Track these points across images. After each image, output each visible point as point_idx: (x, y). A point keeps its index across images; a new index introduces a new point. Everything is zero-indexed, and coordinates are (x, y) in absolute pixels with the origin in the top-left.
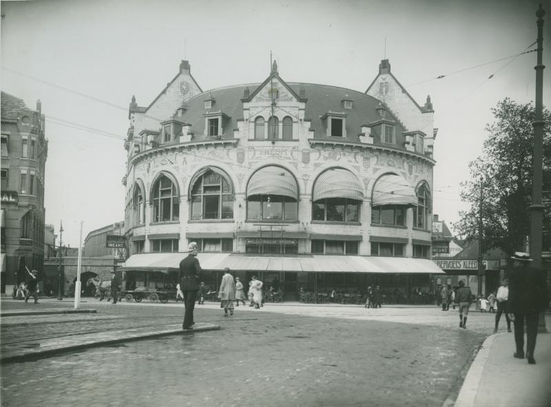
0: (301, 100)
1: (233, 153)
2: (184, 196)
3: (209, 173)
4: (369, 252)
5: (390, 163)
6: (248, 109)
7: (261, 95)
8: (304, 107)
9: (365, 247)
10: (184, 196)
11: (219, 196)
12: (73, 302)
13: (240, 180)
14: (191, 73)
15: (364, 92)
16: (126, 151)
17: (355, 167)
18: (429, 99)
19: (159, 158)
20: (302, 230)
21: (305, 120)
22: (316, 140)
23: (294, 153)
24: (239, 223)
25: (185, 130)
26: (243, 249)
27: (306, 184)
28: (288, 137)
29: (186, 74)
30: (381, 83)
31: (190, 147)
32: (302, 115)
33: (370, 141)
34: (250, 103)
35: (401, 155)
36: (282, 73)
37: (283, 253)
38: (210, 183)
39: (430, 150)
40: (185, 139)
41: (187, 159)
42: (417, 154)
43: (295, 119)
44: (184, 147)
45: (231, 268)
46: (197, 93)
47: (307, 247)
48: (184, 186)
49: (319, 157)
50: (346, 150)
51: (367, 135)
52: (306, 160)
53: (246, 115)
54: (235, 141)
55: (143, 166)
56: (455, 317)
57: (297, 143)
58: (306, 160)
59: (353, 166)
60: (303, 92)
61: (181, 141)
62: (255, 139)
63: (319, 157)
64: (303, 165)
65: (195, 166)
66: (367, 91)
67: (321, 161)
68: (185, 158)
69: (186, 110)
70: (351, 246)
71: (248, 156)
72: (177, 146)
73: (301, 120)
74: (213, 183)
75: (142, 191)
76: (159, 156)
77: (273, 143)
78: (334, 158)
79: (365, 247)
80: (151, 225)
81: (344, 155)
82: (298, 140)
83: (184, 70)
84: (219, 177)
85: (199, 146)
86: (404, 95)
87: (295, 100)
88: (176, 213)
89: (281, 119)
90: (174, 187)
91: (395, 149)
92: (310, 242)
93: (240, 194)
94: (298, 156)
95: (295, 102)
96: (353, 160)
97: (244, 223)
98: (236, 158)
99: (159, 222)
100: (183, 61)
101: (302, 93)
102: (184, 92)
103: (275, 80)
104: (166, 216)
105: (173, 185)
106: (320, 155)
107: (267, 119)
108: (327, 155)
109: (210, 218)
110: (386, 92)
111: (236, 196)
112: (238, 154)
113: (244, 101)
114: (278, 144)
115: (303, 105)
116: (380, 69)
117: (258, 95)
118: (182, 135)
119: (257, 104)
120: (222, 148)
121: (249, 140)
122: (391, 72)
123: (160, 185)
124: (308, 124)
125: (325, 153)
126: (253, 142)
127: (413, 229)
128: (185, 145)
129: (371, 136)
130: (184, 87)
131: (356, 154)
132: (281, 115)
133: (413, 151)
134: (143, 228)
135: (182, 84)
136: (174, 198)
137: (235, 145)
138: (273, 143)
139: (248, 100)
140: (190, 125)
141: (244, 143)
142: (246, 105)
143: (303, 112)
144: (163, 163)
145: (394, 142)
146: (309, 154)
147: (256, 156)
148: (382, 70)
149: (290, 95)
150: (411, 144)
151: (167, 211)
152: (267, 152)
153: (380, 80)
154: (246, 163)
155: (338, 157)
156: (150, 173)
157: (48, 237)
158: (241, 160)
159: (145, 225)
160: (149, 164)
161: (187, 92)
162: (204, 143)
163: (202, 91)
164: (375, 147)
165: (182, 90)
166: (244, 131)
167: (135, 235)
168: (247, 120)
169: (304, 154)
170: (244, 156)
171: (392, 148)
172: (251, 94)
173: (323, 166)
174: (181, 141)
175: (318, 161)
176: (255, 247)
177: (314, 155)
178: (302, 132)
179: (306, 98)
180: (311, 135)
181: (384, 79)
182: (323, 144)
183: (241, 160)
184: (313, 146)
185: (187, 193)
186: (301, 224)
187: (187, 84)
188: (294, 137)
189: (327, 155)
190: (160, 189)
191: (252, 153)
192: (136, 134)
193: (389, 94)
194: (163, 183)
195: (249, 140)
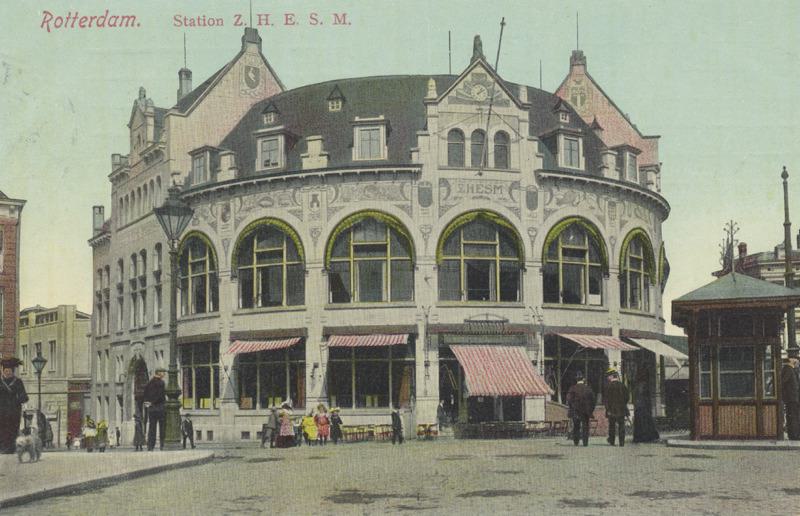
1: (411, 189)
7: (458, 93)
12: (373, 405)
13: (424, 234)
15: (553, 91)
22: (549, 171)
28: (503, 160)
41: (319, 198)
42: (623, 183)
48: (226, 253)
52: (532, 202)
57: (518, 175)
58: (532, 202)
59: (290, 211)
64: (529, 211)
66: (559, 90)
68: (315, 196)
89: (468, 134)
94: (520, 197)
100: (574, 52)
106: (552, 195)
114: (486, 175)
125: (561, 193)
130: (251, 75)
133: (617, 178)
135: (248, 68)
136: (349, 262)
141: (430, 175)
156: (231, 221)
165: (249, 81)
173: (559, 212)
174: (305, 167)
175: (336, 205)
177: (542, 195)
178: (526, 156)
182: (374, 172)
183: (425, 198)
184: (542, 181)
187: (256, 71)
194: (198, 244)
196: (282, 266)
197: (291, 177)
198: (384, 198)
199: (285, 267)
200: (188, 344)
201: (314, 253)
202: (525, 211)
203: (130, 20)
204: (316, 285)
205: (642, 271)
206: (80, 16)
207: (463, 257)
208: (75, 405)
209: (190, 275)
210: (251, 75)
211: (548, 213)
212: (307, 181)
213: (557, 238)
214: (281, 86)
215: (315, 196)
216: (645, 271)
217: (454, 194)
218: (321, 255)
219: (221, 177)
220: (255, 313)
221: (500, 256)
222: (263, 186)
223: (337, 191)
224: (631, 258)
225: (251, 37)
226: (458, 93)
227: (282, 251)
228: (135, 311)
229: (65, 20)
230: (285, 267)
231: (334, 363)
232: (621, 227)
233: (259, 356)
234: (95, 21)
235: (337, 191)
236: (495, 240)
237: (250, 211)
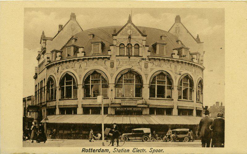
1: (108, 63)
2: (80, 85)
3: (95, 73)
4: (177, 114)
5: (186, 68)
8: (145, 39)
9: (80, 110)
10: (80, 85)
16: (37, 61)
17: (171, 71)
19: (65, 65)
21: (146, 46)
24: (112, 99)
25: (81, 50)
26: (113, 113)
27: (146, 79)
30: (176, 28)
31: (84, 60)
33: (178, 57)
35: (191, 64)
36: (134, 21)
37: (123, 114)
38: (94, 78)
39: (202, 62)
40: (80, 55)
43: (140, 45)
44: (75, 60)
45: (116, 123)
46: (80, 31)
47: (147, 112)
49: (153, 66)
50: (166, 61)
51: (176, 54)
54: (109, 56)
55: (55, 69)
56: (87, 142)
58: (146, 67)
60: (144, 31)
61: (78, 56)
62: (120, 56)
63: (153, 66)
66: (169, 31)
67: (154, 67)
69: (77, 39)
70: (169, 111)
71: (116, 64)
72: (76, 59)
73: (144, 46)
74: (96, 78)
75: (54, 82)
76: (64, 63)
77: (129, 58)
79: (80, 110)
80: (60, 100)
84: (100, 76)
85: (89, 59)
86: (188, 34)
87: (140, 35)
88: (76, 93)
90: (74, 80)
92: (149, 109)
95: (140, 36)
97: (114, 99)
98: (109, 65)
99: (65, 98)
101: (143, 32)
102: (73, 30)
103: (129, 25)
104: (69, 96)
105: (74, 79)
107: (126, 45)
108: (157, 64)
109: (72, 95)
110: (179, 32)
111: (110, 85)
113: (113, 35)
117: (121, 32)
118: (78, 53)
119: (120, 38)
120: (102, 60)
121: (116, 56)
122: (181, 22)
123: (65, 79)
125: (157, 63)
126: (119, 57)
127: (196, 102)
128: (81, 58)
129: (178, 55)
132: (133, 43)
134: (54, 102)
137: (109, 59)
138: (129, 58)
139: (116, 35)
140: (83, 48)
141: (113, 58)
144: (67, 67)
147: (120, 64)
149: (138, 33)
150: (195, 59)
151: (68, 93)
153: (175, 26)
156: (59, 73)
158: (112, 66)
159: (56, 100)
160: (58, 68)
162: (72, 59)
163: (82, 30)
166: (114, 51)
167: (48, 105)
168: (115, 45)
170: (114, 65)
172: (117, 32)
174: (78, 56)
175: (153, 67)
176: (121, 111)
179: (146, 34)
181: (177, 25)
183: (112, 66)
185: (82, 83)
186: (144, 100)
189: (157, 64)
190: (91, 79)
191: (118, 63)
192: (48, 51)
195: (116, 56)
196: (90, 85)
198: (166, 67)
199: (72, 87)
201: (80, 82)
202: (109, 68)
204: (81, 92)
205: (189, 87)
206: (93, 149)
208: (195, 112)
209: (65, 86)
211: (152, 69)
212: (78, 60)
213: (156, 76)
216: (190, 87)
217: (121, 63)
218: (148, 82)
219: (78, 55)
220: (90, 99)
222: (195, 67)
224: (183, 83)
225: (73, 16)
226: (123, 32)
227: (71, 82)
229: (89, 150)
230: (72, 87)
231: (91, 113)
232: (151, 71)
234: (97, 151)
236: (100, 78)
237: (64, 70)
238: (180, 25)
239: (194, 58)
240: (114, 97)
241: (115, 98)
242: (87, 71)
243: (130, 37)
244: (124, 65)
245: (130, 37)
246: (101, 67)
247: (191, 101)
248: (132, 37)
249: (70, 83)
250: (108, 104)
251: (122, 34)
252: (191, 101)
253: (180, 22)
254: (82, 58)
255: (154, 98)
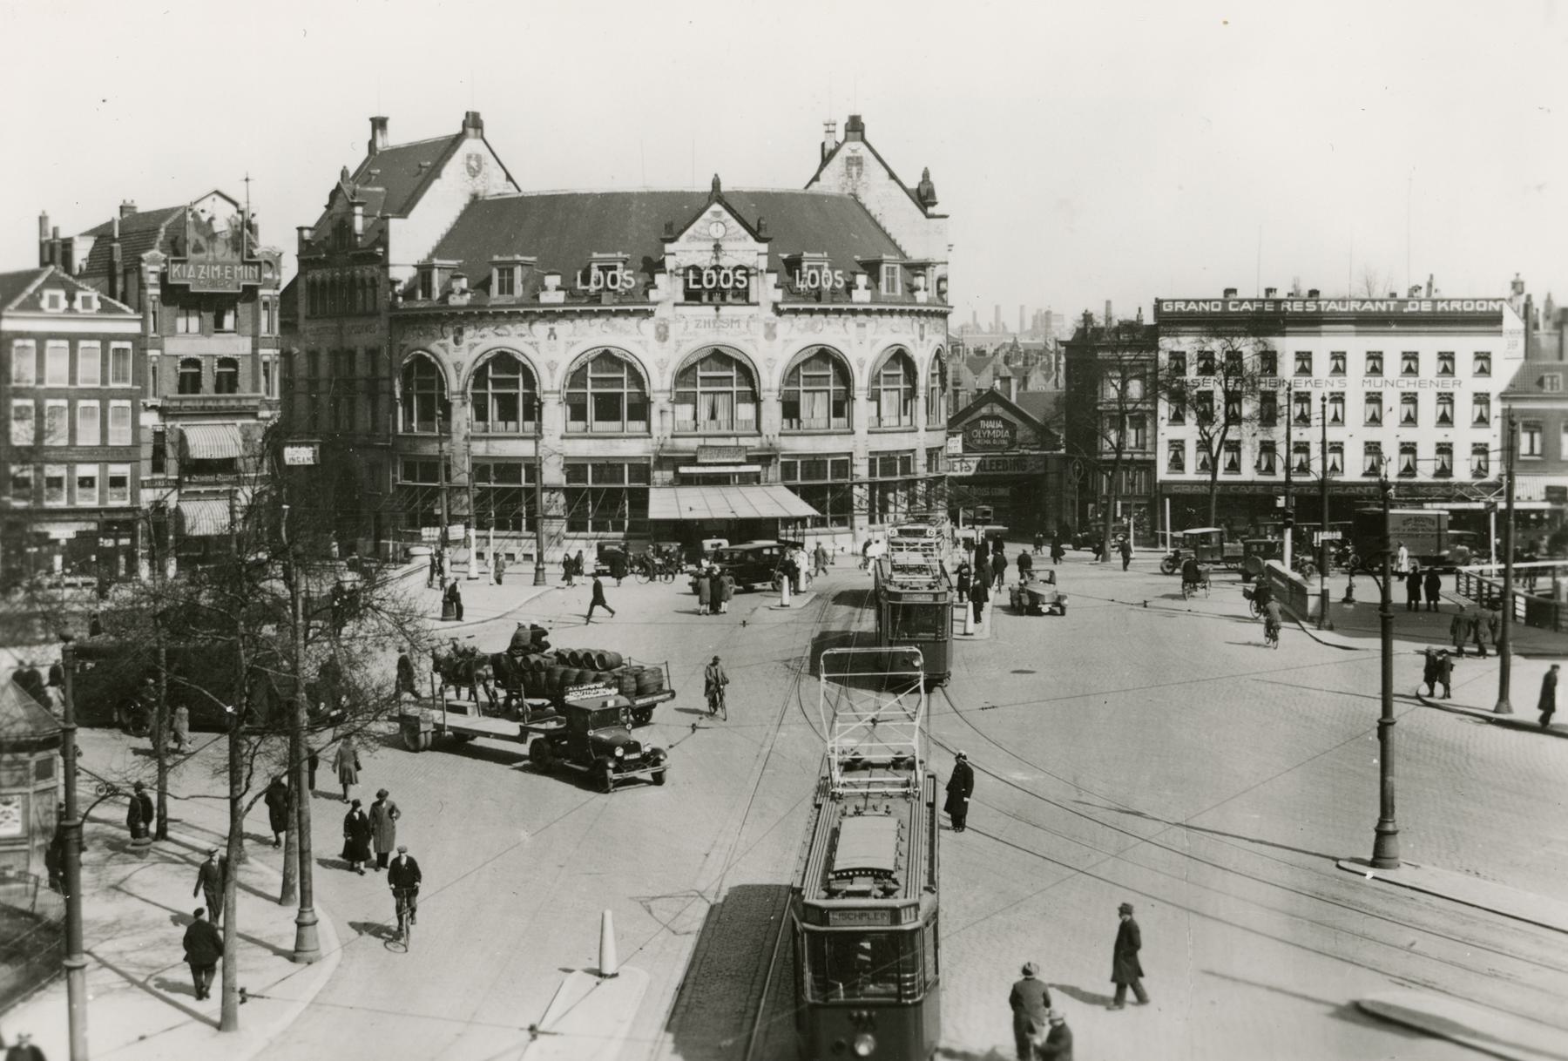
0: (759, 239)
1: (648, 326)
5: (895, 328)
6: (674, 254)
11: (621, 394)
14: (485, 136)
17: (843, 341)
18: (926, 175)
20: (766, 446)
21: (768, 271)
23: (752, 325)
29: (476, 137)
30: (848, 158)
32: (763, 263)
33: (560, 297)
34: (676, 244)
41: (556, 331)
52: (771, 333)
53: (670, 263)
57: (756, 308)
58: (771, 333)
65: (573, 344)
68: (552, 330)
78: (812, 328)
81: (829, 323)
82: (757, 304)
83: (471, 131)
86: (893, 182)
87: (751, 239)
91: (903, 304)
93: (770, 390)
96: (842, 330)
97: (669, 439)
108: (802, 326)
110: (859, 174)
112: (657, 328)
115: (764, 247)
116: (847, 131)
117: (690, 231)
119: (688, 247)
121: (676, 305)
124: (773, 278)
129: (867, 288)
130: (474, 163)
131: (531, 323)
135: (469, 157)
138: (717, 309)
139: (672, 241)
142: (669, 247)
143: (765, 258)
145: (899, 292)
146: (775, 325)
148: (850, 134)
149: (744, 232)
152: (707, 323)
154: (671, 342)
155: (820, 327)
157: (187, 452)
158: (663, 336)
161: (479, 172)
164: (875, 307)
165: (469, 168)
168: (671, 271)
169: (767, 325)
171: (897, 304)
177: (784, 325)
178: (766, 289)
180: (778, 295)
181: (854, 151)
183: (663, 336)
186: (764, 438)
187: (478, 158)
188: (753, 298)
190: (590, 374)
191: (683, 325)
193: (864, 178)
195: (676, 305)
197: (532, 312)
200: (602, 466)
202: (653, 343)
203: (612, 612)
207: (625, 390)
210: (474, 163)
214: (519, 190)
215: (552, 330)
217: (692, 327)
221: (621, 394)
223: (88, 953)
228: (267, 382)
233: (210, 894)
235: (88, 953)
237: (480, 343)
238: (862, 150)
239: (918, 289)
240: (668, 433)
241: (780, 435)
242: (575, 352)
243: (717, 248)
244: (702, 331)
245: (717, 248)
246: (624, 336)
247: (1292, 447)
248: (725, 246)
249: (431, 385)
250: (649, 458)
251: (694, 238)
252: (1292, 447)
253: (863, 139)
254: (561, 309)
255: (429, 434)
